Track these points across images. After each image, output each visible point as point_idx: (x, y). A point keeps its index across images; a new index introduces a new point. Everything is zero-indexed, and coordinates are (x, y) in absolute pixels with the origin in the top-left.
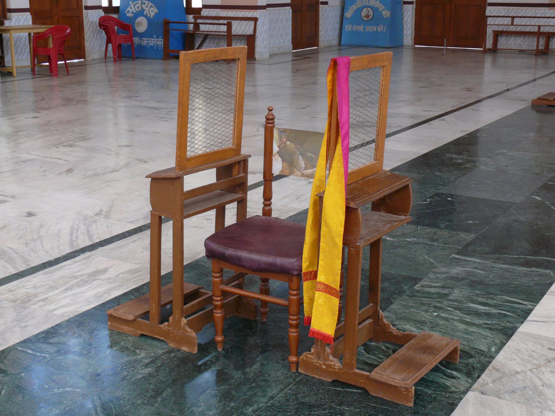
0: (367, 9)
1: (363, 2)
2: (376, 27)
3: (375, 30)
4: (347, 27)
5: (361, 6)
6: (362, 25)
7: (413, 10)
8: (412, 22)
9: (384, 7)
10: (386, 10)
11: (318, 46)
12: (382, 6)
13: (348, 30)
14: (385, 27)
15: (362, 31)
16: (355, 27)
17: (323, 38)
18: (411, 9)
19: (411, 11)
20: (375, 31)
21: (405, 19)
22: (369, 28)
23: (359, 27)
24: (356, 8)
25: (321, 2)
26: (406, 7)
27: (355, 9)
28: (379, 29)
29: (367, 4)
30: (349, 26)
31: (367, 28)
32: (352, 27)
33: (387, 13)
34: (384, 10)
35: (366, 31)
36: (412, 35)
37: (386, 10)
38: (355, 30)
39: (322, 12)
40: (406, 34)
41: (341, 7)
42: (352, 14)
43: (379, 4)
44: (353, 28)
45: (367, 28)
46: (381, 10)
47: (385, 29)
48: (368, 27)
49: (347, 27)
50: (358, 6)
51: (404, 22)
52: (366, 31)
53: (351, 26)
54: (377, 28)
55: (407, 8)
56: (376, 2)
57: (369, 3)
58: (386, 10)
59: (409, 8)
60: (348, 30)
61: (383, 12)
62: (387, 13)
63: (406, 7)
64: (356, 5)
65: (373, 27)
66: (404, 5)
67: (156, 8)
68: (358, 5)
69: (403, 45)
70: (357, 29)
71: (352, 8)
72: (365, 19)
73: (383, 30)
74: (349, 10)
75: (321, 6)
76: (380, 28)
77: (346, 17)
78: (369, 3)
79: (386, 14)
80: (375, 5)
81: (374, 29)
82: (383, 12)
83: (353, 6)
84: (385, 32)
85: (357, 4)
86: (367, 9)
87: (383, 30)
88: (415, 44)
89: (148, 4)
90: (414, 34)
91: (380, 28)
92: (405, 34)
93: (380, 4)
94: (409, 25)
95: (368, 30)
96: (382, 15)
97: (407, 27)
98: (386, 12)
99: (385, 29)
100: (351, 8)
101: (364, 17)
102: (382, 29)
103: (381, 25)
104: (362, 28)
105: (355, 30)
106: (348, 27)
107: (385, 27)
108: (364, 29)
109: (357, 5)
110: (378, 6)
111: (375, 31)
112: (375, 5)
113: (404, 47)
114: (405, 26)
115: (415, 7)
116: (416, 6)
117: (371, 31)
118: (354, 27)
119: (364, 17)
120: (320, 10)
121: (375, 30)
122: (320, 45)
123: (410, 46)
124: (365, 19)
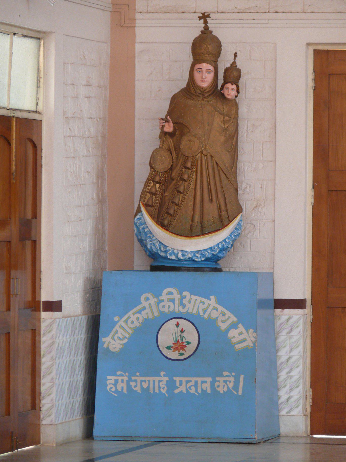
0: (177, 325)
1: (163, 301)
2: (209, 379)
3: (207, 387)
4: (111, 379)
5: (156, 314)
6: (162, 373)
7: (305, 324)
8: (304, 364)
9: (234, 319)
10: (240, 326)
11: (36, 441)
12: (228, 314)
13: (116, 390)
14: (242, 377)
15: (164, 391)
16: (139, 379)
17: (53, 416)
18: (301, 322)
19: (301, 327)
20: (209, 391)
21: (283, 354)
22: (187, 382)
23: (151, 379)
24: (141, 321)
25: (46, 303)
26: (284, 318)
27: (137, 324)
28: (222, 384)
29: (177, 309)
30: (120, 378)
31: (181, 384)
32: (130, 380)
33: (245, 335)
34: (234, 326)
35: (176, 391)
36: (305, 404)
37: (241, 328)
38: (138, 389)
39: (50, 335)
40: (288, 400)
41: (86, 316)
42: (126, 341)
43: (215, 309)
44: (133, 384)
45: (181, 384)
46: (223, 327)
47: (241, 384)
48: (184, 379)
49: (111, 379)
50: (147, 314)
51: (279, 363)
52: (176, 391)
53: (125, 378)
54: (212, 383)
55: (288, 320)
56: (207, 301)
57: (184, 306)
58: (240, 326)
59: (295, 318)
60: (116, 390)
61: (233, 333)
62: (245, 335)
63: (284, 318)
64: (139, 312)
65: (199, 380)
66: (278, 311)
67: (114, 330)
68: (148, 310)
69: (279, 436)
70: (145, 385)
71: (126, 322)
72: (174, 355)
73: (236, 387)
74: (117, 328)
75: (44, 315)
76: (225, 382)
77: (108, 349)
78: (184, 306)
79: (242, 337)
80: (205, 311)
81: (204, 386)
82: (233, 333)
83: (130, 313)
84: (240, 393)
85: (144, 308)
86: (177, 325)
87: (236, 387)
88: (312, 433)
89: (229, 317)
90: (309, 400)
91: (225, 382)
92: (283, 398)
93: (220, 308)
94: (296, 374)
95: (183, 389)
96: (228, 342)
97: (291, 377)
98: (241, 334)
99: (241, 384)
100: (121, 323)
101: (168, 348)
102: (231, 385)
103: (225, 373)
104: (162, 385)
105: (138, 389)
106: (116, 381)
107: (242, 377)
108: (171, 385)
109: (143, 313)
110: (214, 315)
111: (209, 391)
112: (205, 311)
113: (281, 440)
114: (283, 375)
115: (309, 318)
116: (315, 312)
117: (193, 390)
118: (136, 381)
119: (168, 348)
120: (43, 326)
121: (207, 387)
122: (43, 439)
123: (302, 437)
124: (174, 355)
